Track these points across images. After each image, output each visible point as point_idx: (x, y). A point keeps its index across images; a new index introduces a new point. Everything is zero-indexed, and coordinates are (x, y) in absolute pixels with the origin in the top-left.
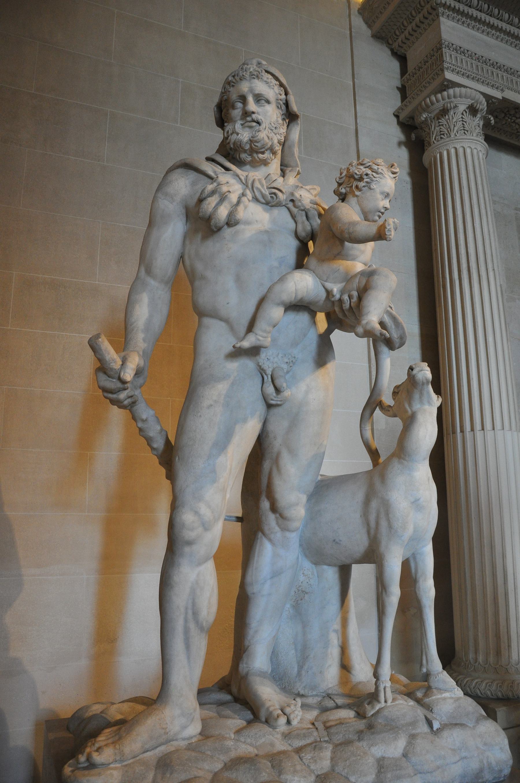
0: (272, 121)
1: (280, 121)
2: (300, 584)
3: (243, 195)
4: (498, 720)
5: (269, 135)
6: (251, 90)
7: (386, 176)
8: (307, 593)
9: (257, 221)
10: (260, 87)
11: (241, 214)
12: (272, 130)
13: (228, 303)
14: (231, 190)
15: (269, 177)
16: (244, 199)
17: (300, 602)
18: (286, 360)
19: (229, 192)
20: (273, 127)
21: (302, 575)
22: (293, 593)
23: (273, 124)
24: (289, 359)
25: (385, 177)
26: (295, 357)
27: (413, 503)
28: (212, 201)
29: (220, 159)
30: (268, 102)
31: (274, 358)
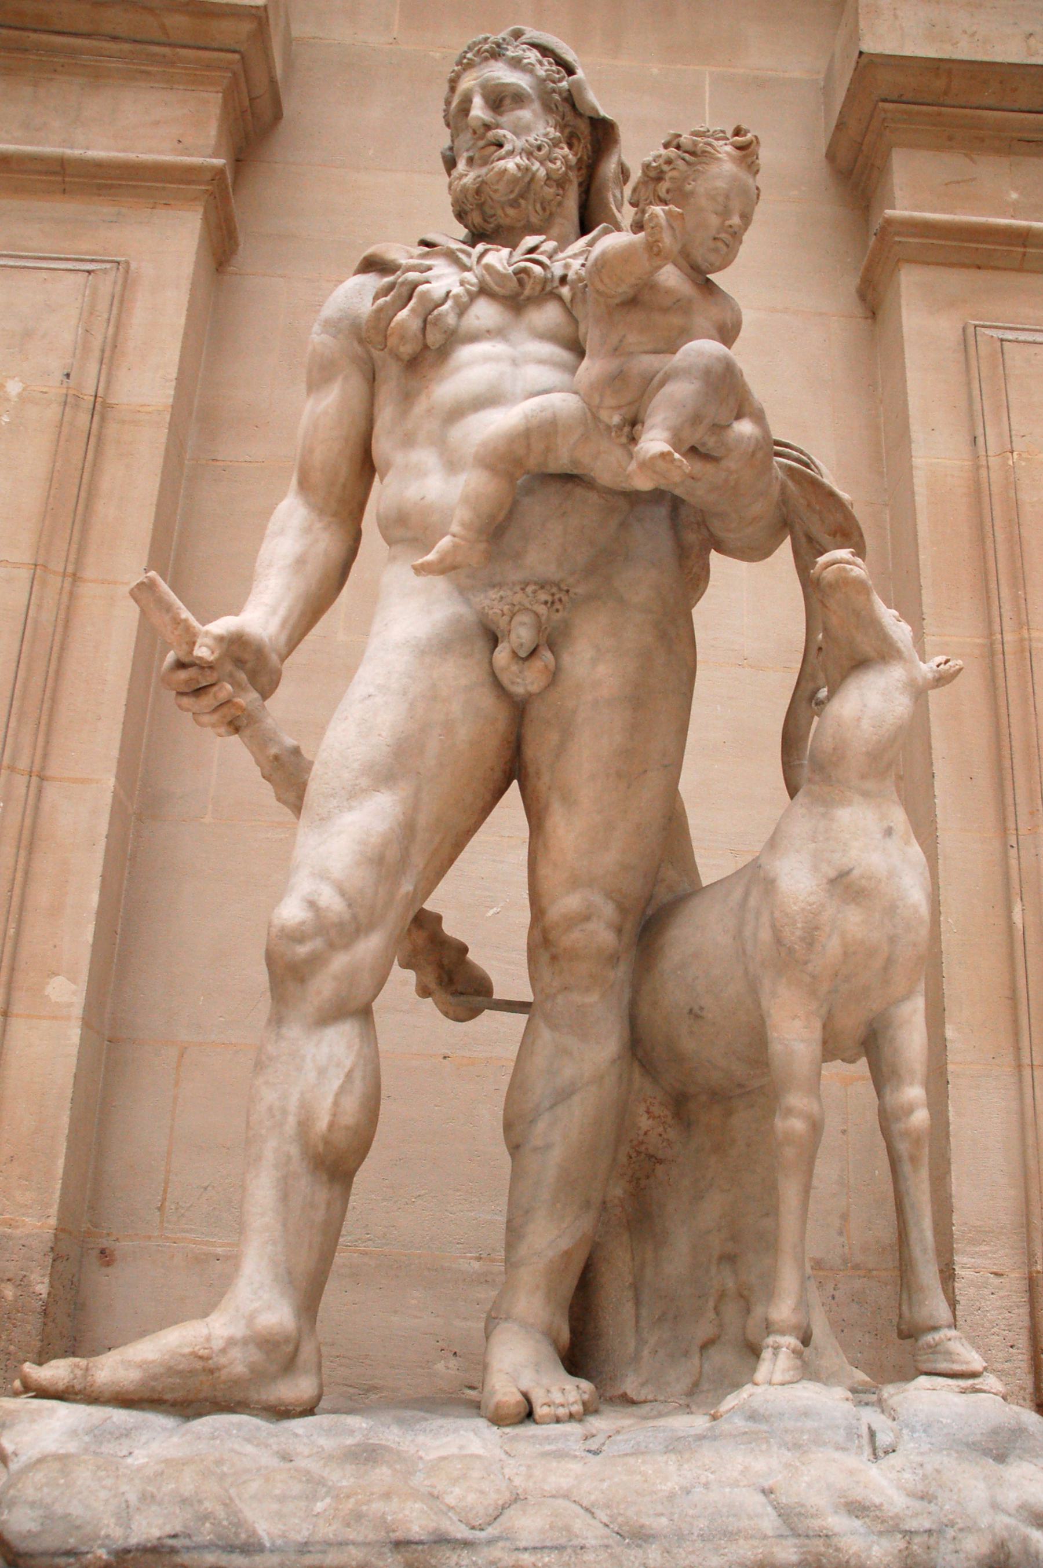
2: (641, 1138)
4: (867, 558)
8: (660, 1161)
15: (867, 1450)
17: (643, 1183)
21: (646, 1116)
22: (623, 1158)
24: (553, 595)
27: (832, 882)
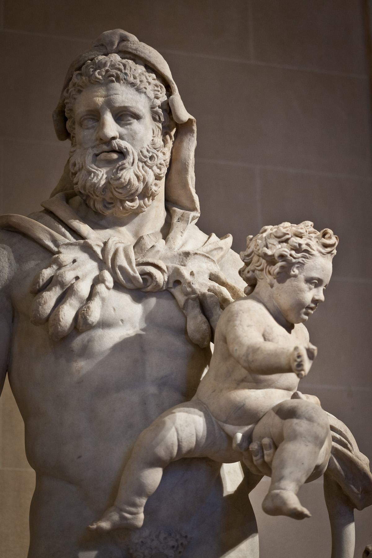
0: (145, 146)
1: (159, 141)
3: (98, 280)
5: (140, 174)
6: (109, 104)
7: (313, 252)
9: (122, 320)
10: (124, 96)
11: (95, 313)
12: (145, 162)
13: (79, 457)
14: (79, 275)
16: (101, 288)
18: (172, 543)
19: (77, 278)
20: (145, 157)
23: (146, 153)
24: (177, 540)
25: (312, 255)
26: (186, 537)
28: (50, 297)
29: (62, 211)
30: (137, 117)
31: (153, 540)
